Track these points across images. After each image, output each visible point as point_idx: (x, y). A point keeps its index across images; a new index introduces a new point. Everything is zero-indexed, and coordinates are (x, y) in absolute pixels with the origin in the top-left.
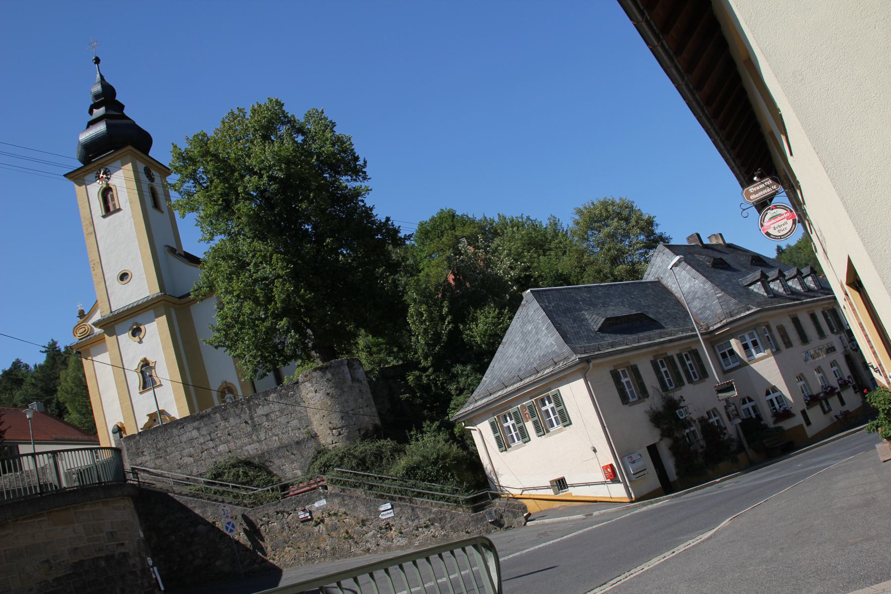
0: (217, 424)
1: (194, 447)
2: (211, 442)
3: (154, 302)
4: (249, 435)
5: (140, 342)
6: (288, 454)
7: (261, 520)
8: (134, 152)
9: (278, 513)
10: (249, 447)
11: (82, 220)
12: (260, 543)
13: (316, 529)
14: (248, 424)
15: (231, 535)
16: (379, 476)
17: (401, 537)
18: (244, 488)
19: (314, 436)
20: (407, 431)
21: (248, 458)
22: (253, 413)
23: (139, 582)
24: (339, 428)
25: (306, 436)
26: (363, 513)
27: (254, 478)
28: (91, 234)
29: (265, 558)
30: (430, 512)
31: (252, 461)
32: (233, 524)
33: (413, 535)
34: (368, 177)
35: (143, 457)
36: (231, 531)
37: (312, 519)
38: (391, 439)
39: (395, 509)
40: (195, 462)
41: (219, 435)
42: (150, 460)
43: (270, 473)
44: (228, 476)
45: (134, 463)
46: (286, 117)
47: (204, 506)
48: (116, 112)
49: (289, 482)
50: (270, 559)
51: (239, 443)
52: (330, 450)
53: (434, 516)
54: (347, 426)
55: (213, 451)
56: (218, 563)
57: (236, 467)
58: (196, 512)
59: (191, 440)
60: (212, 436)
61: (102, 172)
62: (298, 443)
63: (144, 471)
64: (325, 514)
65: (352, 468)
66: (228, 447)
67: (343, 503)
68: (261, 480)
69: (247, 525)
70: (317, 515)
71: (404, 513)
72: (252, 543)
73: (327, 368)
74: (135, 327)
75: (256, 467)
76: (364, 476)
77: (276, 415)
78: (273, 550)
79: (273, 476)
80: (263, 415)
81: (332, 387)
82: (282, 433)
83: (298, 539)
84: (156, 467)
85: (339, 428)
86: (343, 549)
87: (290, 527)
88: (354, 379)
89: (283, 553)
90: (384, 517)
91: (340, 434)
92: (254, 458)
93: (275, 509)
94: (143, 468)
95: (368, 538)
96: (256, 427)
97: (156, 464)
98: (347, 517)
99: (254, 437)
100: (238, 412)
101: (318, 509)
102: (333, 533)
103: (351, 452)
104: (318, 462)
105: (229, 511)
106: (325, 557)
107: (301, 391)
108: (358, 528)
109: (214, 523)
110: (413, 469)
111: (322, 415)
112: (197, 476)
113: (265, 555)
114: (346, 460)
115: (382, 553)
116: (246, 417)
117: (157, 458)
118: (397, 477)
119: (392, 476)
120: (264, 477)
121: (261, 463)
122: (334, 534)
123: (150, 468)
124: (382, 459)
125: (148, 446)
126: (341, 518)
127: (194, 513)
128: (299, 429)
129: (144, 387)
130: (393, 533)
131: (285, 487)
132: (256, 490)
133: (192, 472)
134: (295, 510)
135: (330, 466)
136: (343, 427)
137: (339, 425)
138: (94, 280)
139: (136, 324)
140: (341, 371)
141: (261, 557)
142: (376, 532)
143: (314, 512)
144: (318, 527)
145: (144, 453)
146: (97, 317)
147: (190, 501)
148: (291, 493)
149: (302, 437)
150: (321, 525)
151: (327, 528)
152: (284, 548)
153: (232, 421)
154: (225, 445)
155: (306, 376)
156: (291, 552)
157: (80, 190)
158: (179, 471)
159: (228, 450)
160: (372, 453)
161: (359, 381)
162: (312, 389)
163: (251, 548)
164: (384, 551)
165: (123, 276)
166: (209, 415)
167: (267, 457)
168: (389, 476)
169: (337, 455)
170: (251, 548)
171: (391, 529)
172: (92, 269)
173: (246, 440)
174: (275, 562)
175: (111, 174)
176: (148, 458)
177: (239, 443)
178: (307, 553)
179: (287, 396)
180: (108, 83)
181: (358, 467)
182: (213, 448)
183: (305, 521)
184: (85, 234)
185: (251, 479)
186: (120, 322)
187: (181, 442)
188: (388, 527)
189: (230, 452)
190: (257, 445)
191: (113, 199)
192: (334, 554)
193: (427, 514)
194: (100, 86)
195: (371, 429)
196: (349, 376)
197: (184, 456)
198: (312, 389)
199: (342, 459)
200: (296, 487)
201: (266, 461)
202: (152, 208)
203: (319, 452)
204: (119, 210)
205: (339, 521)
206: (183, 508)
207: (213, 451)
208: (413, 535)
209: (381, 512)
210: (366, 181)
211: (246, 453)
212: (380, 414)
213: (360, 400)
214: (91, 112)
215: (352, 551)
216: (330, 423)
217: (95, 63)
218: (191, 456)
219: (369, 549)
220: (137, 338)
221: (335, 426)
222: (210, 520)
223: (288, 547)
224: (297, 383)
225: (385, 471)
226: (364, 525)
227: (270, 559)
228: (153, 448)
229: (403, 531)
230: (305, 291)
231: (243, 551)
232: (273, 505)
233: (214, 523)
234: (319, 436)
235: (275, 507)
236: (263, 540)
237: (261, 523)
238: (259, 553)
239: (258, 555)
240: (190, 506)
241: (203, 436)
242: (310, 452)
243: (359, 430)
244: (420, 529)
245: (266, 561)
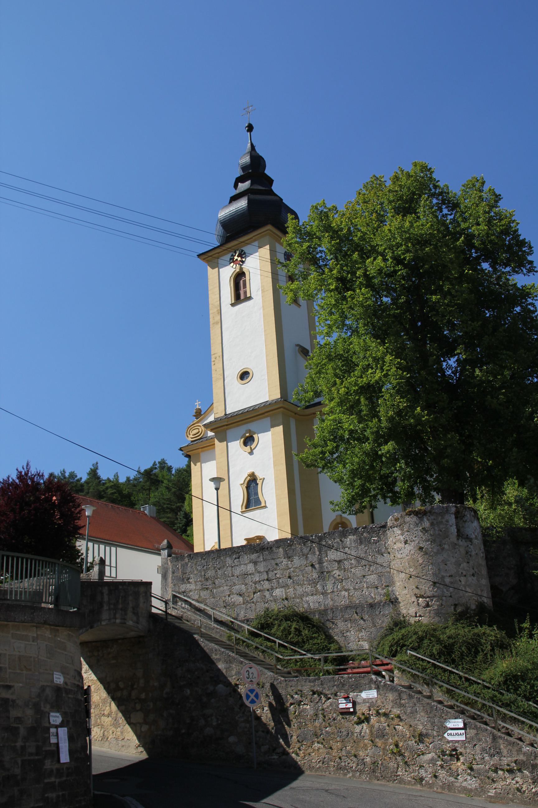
0: (278, 561)
1: (246, 584)
2: (267, 582)
3: (272, 408)
4: (314, 583)
5: (251, 453)
6: (357, 617)
7: (292, 697)
8: (274, 233)
9: (314, 693)
10: (310, 599)
11: (210, 306)
12: (285, 728)
13: (358, 728)
14: (315, 568)
15: (252, 707)
16: (466, 675)
17: (469, 775)
18: (292, 649)
19: (394, 602)
20: (516, 620)
21: (306, 612)
22: (323, 556)
23: (19, 744)
24: (428, 597)
25: (383, 599)
26: (422, 723)
27: (308, 640)
28: (217, 323)
29: (287, 749)
30: (520, 750)
31: (311, 616)
32: (257, 693)
33: (488, 778)
34: (536, 270)
35: (188, 585)
36: (253, 702)
37: (354, 713)
38: (498, 628)
39: (468, 730)
40: (244, 603)
41: (278, 576)
42: (195, 590)
43: (330, 639)
44: (277, 630)
45: (177, 589)
46: (436, 187)
47: (229, 661)
48: (263, 187)
49: (350, 653)
50: (293, 752)
51: (300, 590)
52: (410, 624)
53: (524, 759)
54: (439, 597)
55: (267, 594)
56: (232, 739)
57: (289, 620)
58: (220, 667)
59: (246, 575)
60: (270, 576)
61: (237, 254)
62: (371, 606)
63: (186, 601)
64: (373, 712)
65: (431, 656)
66: (286, 593)
67: (398, 701)
68: (314, 644)
69: (275, 699)
70: (362, 709)
71: (480, 740)
72: (275, 725)
73: (425, 513)
74: (248, 435)
75: (314, 626)
76: (445, 670)
77: (351, 564)
78: (298, 741)
79: (333, 642)
80: (335, 561)
81: (428, 540)
82: (354, 589)
83: (332, 736)
84: (200, 600)
85: (428, 597)
86: (387, 768)
87: (325, 717)
88: (460, 534)
89: (310, 750)
90: (450, 738)
91: (428, 605)
92: (314, 613)
93: (311, 686)
94: (185, 598)
95: (424, 762)
96: (323, 574)
97: (200, 596)
98: (401, 724)
99: (319, 587)
100: (305, 550)
101: (365, 701)
102: (377, 740)
103: (437, 633)
104: (390, 638)
105: (256, 675)
106: (361, 772)
107: (387, 539)
108: (412, 743)
109: (237, 685)
110: (516, 678)
112: (242, 621)
113: (288, 745)
114: (426, 642)
115: (439, 790)
116: (313, 558)
117: (203, 589)
118: (490, 683)
119: (484, 681)
120: (319, 641)
121: (320, 622)
122: (379, 742)
123: (193, 600)
124: (477, 653)
125: (195, 572)
126: (393, 722)
127: (217, 666)
128: (377, 588)
129: (248, 506)
130: (459, 765)
131: (342, 661)
132: (305, 655)
133: (238, 615)
134: (336, 695)
135: (404, 645)
136: (434, 596)
137: (429, 594)
138: (213, 376)
139: (250, 431)
140: (444, 520)
141: (282, 746)
142: (436, 757)
143: (359, 704)
144: (360, 726)
145: (191, 580)
147: (216, 650)
148: (349, 671)
149: (378, 598)
150: (365, 725)
151: (371, 731)
152: (313, 743)
153: (297, 561)
154: (283, 589)
155: (396, 520)
156: (321, 751)
157: (212, 273)
158: (224, 610)
159: (284, 597)
160: (464, 642)
161: (468, 539)
162: (402, 538)
163: (273, 731)
164: (443, 787)
165: (244, 375)
166: (271, 548)
167: (330, 616)
168: (480, 679)
169: (416, 633)
170: (273, 731)
171: (458, 759)
172: (213, 363)
173: (309, 589)
174: (298, 759)
175: (245, 257)
176: (193, 587)
177: (300, 590)
178: (340, 758)
179: (369, 542)
180: (258, 154)
181: (440, 657)
182: (268, 590)
183: (345, 713)
184: (211, 323)
185: (303, 639)
186: (234, 427)
187: (233, 576)
188: (455, 754)
189: (287, 599)
190: (320, 598)
191: (245, 286)
192: (374, 771)
193: (515, 753)
194: (249, 157)
195: (473, 607)
196: (454, 530)
197: (233, 594)
198: (402, 538)
199: (421, 639)
200: (356, 663)
201: (328, 620)
203: (396, 624)
204: (250, 298)
205: (388, 725)
206: (206, 658)
207: (267, 594)
208: (488, 778)
210: (531, 274)
211: (306, 606)
212: (495, 590)
213: (464, 565)
214: (236, 186)
215: (398, 773)
216: (417, 588)
217: (248, 131)
218: (240, 595)
219: (422, 779)
221: (423, 593)
222: (233, 680)
223: (318, 743)
224: (384, 526)
225: (477, 671)
226: (421, 741)
227: (293, 752)
228: (201, 576)
229: (475, 767)
230: (422, 410)
231: (263, 732)
232: (310, 682)
233: (237, 685)
234: (400, 603)
235: (312, 684)
236: (289, 725)
237: (291, 701)
238: (281, 740)
239: (279, 743)
240: (214, 657)
241: (259, 572)
242: (384, 621)
243: (456, 605)
244: (500, 772)
245: (288, 754)
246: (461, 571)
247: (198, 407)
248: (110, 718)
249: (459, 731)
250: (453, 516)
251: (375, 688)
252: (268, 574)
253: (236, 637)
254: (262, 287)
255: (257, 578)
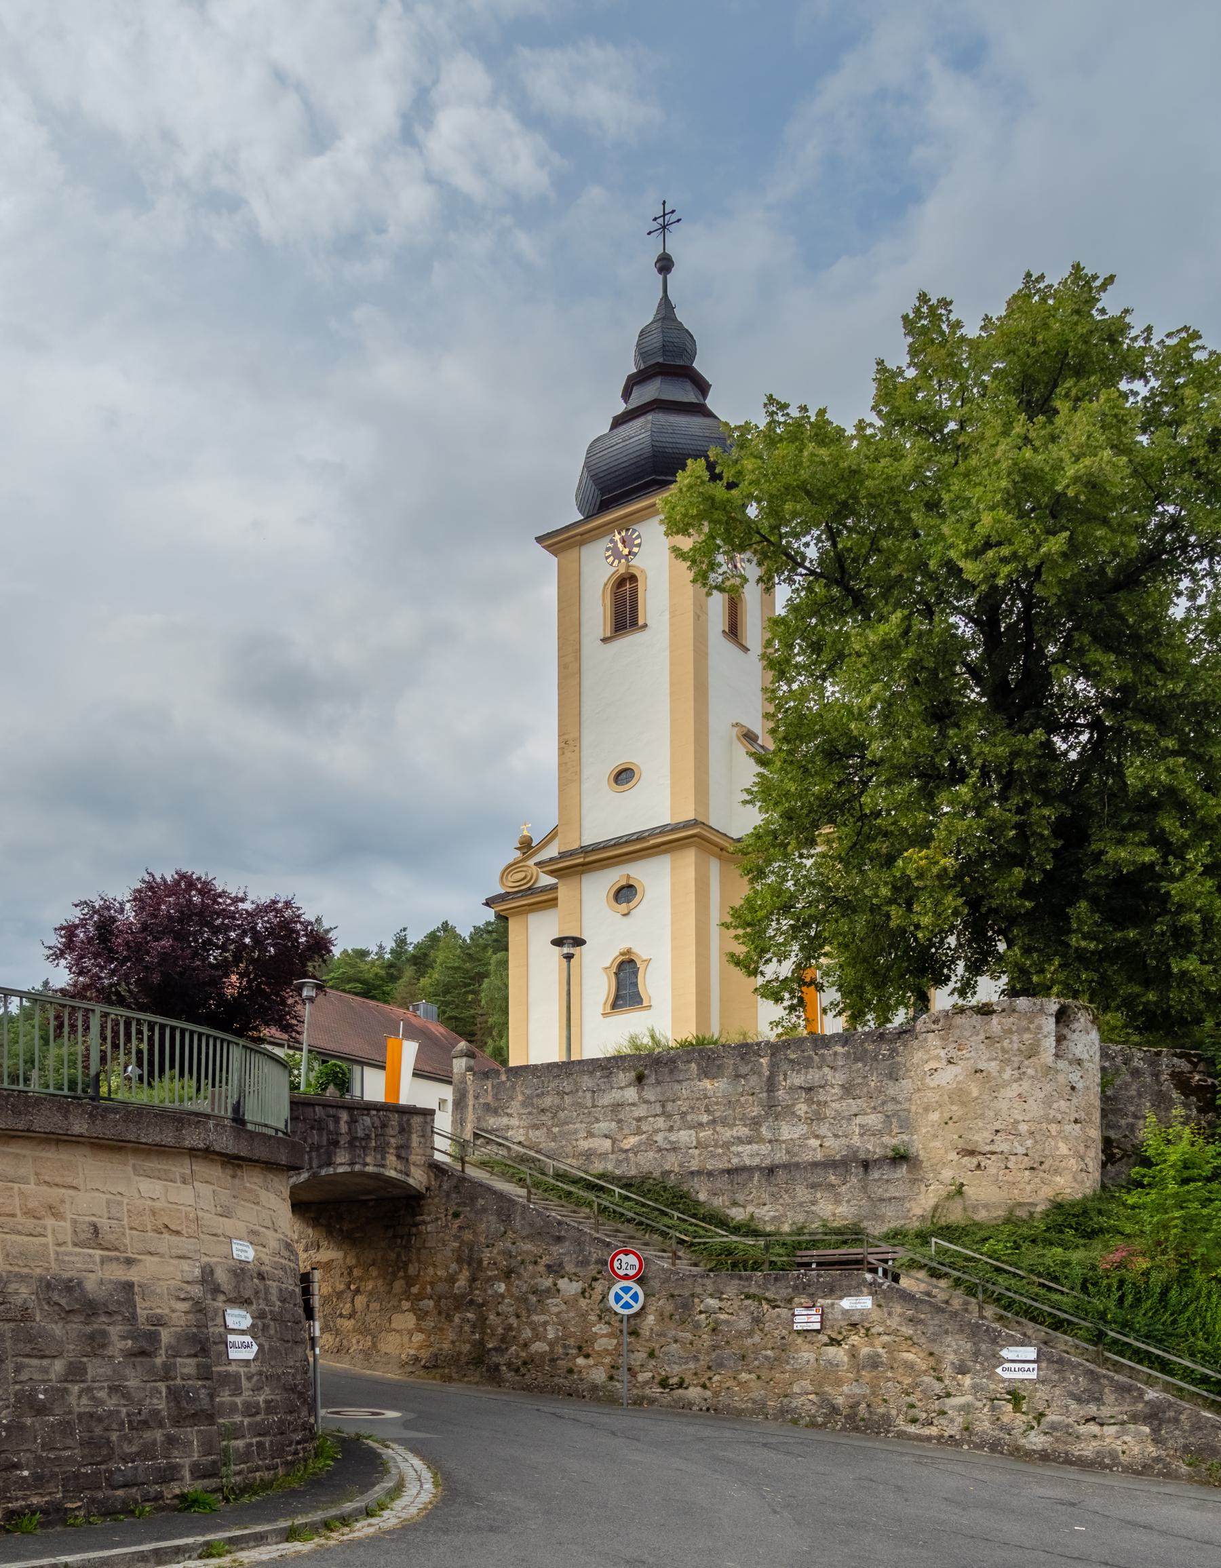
40: (613, 1152)
59: (617, 1106)
80: (801, 1088)
90: (1007, 1375)
97: (528, 1138)
111: (946, 1116)
146: (552, 851)
159: (694, 1144)
165: (623, 776)
173: (743, 1131)
176: (514, 1122)
198: (942, 1053)
202: (721, 635)
209: (1002, 1361)
220: (624, 907)
232: (741, 1278)
234: (922, 1162)
241: (647, 1102)
246: (1052, 1113)
247: (525, 833)
248: (352, 1321)
249: (1026, 1366)
250: (1052, 1020)
251: (870, 1294)
252: (663, 1106)
253: (599, 1205)
254: (671, 606)
255: (640, 1111)
